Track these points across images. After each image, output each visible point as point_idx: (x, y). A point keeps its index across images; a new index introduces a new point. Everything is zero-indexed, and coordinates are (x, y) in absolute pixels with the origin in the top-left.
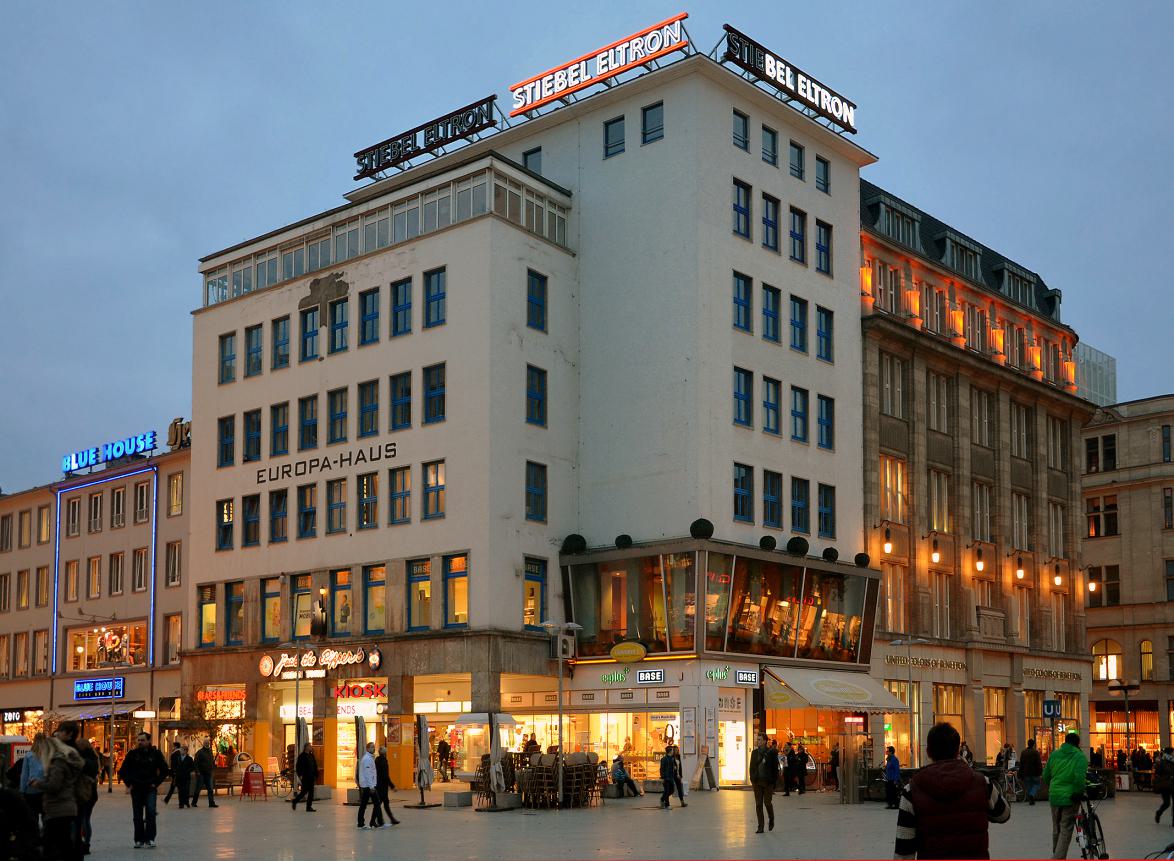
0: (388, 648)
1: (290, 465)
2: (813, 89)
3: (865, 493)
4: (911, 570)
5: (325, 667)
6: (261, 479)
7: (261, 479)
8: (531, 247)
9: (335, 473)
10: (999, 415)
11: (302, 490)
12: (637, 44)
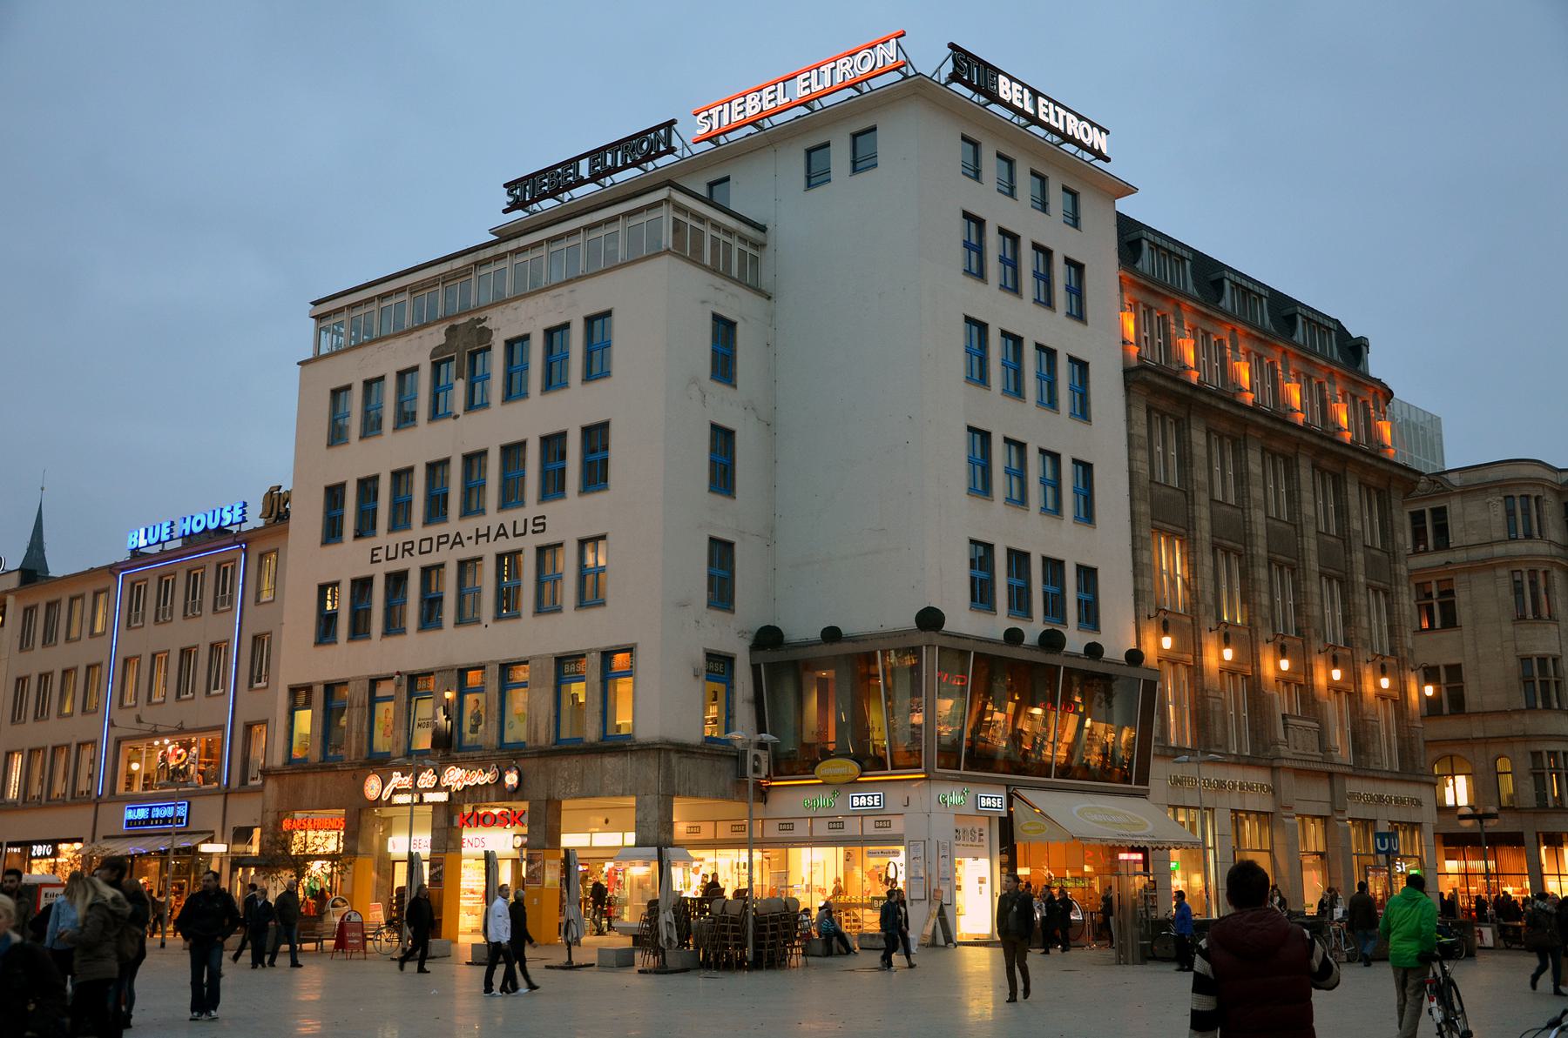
0: (530, 764)
1: (412, 542)
2: (1056, 113)
3: (1135, 576)
4: (1196, 670)
5: (448, 788)
6: (375, 559)
7: (375, 559)
8: (717, 289)
9: (468, 551)
10: (1299, 482)
11: (426, 571)
12: (844, 64)
